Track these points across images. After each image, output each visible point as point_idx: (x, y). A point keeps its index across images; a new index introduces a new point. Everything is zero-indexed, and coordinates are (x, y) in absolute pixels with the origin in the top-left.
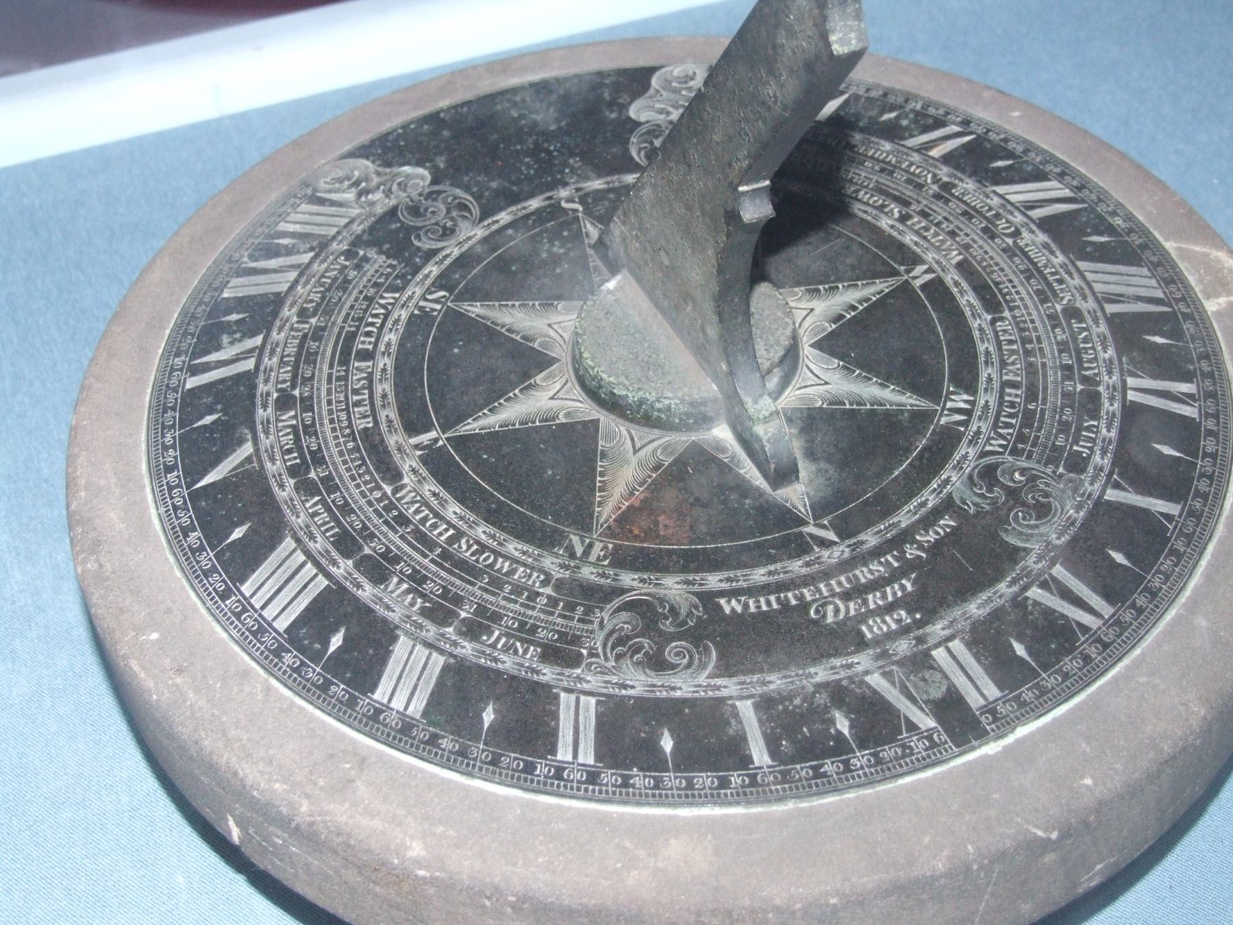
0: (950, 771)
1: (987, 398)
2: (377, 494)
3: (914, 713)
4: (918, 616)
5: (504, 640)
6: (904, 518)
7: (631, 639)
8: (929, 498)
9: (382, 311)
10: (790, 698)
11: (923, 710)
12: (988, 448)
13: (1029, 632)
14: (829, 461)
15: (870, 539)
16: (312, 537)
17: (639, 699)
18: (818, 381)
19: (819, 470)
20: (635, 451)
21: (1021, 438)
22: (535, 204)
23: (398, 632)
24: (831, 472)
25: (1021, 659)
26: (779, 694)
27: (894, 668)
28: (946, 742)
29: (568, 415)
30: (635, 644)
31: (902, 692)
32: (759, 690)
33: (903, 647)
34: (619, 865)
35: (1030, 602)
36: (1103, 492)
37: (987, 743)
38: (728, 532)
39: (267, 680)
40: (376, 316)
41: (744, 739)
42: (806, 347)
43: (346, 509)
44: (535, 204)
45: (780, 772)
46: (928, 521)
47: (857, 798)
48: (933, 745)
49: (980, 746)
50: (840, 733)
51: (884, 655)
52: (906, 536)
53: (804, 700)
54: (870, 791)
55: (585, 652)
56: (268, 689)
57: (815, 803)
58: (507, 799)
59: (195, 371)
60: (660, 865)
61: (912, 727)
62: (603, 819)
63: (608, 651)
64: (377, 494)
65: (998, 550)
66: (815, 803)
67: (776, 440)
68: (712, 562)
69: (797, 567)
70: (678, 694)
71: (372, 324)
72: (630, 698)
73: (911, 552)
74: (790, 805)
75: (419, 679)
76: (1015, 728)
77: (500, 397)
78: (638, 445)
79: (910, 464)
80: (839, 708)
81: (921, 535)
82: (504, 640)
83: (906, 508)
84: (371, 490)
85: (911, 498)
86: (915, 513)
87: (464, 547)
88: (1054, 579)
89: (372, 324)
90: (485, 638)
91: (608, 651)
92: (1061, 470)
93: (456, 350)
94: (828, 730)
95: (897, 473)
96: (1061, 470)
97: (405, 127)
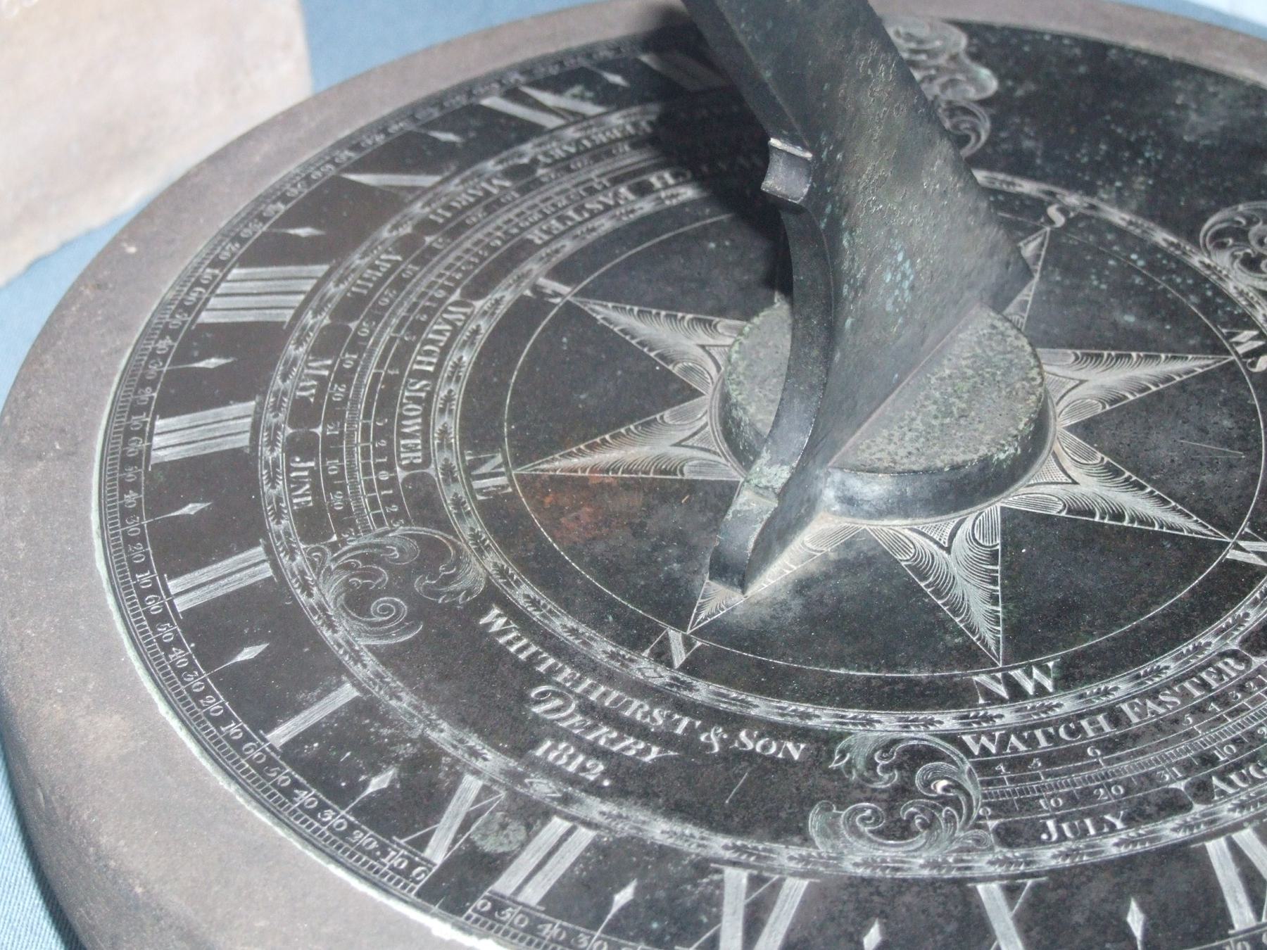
0: (378, 907)
1: (1067, 704)
2: (384, 476)
3: (445, 836)
4: (606, 783)
5: (306, 473)
6: (762, 707)
7: (379, 563)
8: (824, 718)
9: (448, 327)
10: (385, 722)
11: (455, 841)
12: (967, 739)
13: (661, 894)
14: (806, 606)
15: (703, 691)
16: (340, 281)
17: (297, 607)
18: (690, 442)
19: (784, 603)
20: (948, 550)
21: (1018, 763)
22: (1027, 187)
23: (258, 398)
24: (790, 614)
25: (608, 902)
26: (387, 713)
27: (503, 794)
28: (417, 882)
29: (688, 370)
30: (372, 569)
31: (468, 815)
32: (378, 692)
33: (542, 788)
34: (60, 691)
35: (716, 877)
36: (988, 879)
37: (443, 919)
38: (609, 572)
39: (128, 345)
40: (440, 332)
41: (297, 712)
42: (999, 505)
43: (400, 284)
44: (1027, 187)
45: (270, 758)
46: (776, 731)
47: (281, 839)
48: (406, 873)
49: (434, 915)
50: (365, 784)
51: (516, 777)
52: (733, 722)
53: (391, 737)
54: (299, 847)
55: (335, 538)
56: (119, 351)
57: (249, 808)
58: (93, 572)
59: (513, 94)
60: (81, 722)
61: (422, 843)
62: (113, 651)
63: (349, 555)
64: (384, 476)
65: (783, 815)
66: (249, 808)
67: (744, 519)
68: (548, 573)
69: (602, 648)
70: (327, 634)
71: (433, 342)
72: (294, 599)
73: (714, 738)
74: (232, 789)
75: (215, 438)
76: (487, 936)
77: (666, 308)
78: (945, 541)
79: (869, 679)
80: (401, 769)
81: (749, 736)
82: (306, 473)
83: (784, 704)
84: (379, 467)
85: (808, 700)
86: (782, 715)
87: (418, 386)
88: (776, 887)
89: (433, 342)
90: (298, 459)
91: (349, 555)
92: (992, 824)
93: (712, 245)
94: (361, 772)
95: (842, 671)
96: (992, 824)
97: (1058, 37)
